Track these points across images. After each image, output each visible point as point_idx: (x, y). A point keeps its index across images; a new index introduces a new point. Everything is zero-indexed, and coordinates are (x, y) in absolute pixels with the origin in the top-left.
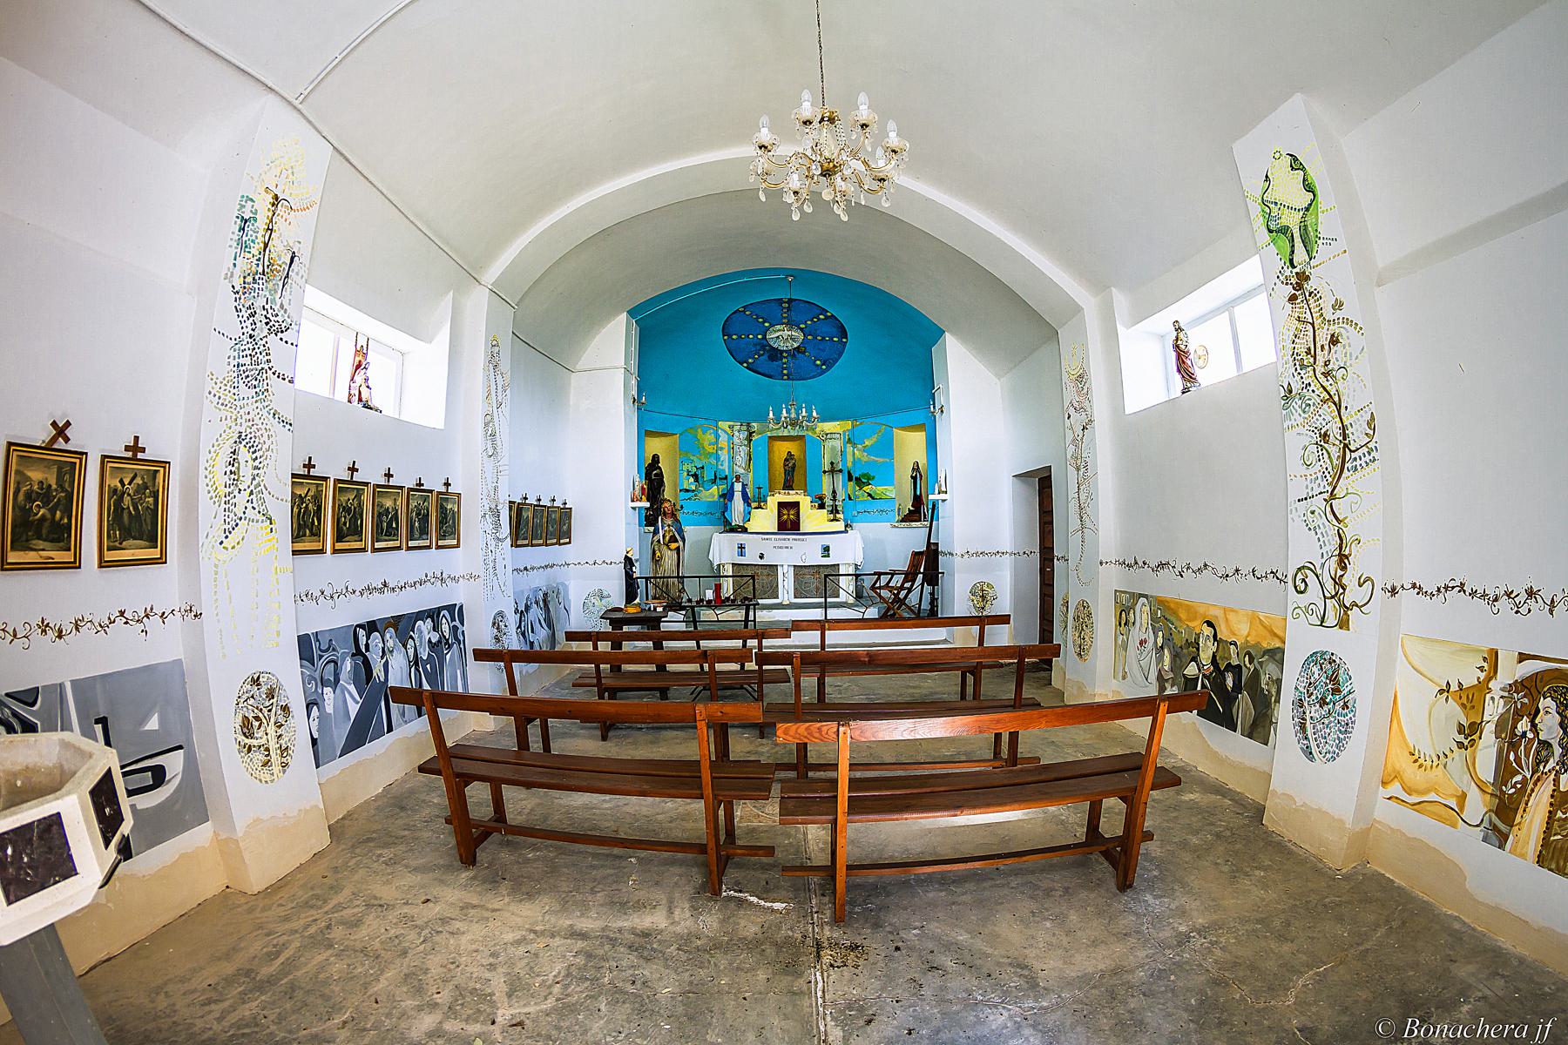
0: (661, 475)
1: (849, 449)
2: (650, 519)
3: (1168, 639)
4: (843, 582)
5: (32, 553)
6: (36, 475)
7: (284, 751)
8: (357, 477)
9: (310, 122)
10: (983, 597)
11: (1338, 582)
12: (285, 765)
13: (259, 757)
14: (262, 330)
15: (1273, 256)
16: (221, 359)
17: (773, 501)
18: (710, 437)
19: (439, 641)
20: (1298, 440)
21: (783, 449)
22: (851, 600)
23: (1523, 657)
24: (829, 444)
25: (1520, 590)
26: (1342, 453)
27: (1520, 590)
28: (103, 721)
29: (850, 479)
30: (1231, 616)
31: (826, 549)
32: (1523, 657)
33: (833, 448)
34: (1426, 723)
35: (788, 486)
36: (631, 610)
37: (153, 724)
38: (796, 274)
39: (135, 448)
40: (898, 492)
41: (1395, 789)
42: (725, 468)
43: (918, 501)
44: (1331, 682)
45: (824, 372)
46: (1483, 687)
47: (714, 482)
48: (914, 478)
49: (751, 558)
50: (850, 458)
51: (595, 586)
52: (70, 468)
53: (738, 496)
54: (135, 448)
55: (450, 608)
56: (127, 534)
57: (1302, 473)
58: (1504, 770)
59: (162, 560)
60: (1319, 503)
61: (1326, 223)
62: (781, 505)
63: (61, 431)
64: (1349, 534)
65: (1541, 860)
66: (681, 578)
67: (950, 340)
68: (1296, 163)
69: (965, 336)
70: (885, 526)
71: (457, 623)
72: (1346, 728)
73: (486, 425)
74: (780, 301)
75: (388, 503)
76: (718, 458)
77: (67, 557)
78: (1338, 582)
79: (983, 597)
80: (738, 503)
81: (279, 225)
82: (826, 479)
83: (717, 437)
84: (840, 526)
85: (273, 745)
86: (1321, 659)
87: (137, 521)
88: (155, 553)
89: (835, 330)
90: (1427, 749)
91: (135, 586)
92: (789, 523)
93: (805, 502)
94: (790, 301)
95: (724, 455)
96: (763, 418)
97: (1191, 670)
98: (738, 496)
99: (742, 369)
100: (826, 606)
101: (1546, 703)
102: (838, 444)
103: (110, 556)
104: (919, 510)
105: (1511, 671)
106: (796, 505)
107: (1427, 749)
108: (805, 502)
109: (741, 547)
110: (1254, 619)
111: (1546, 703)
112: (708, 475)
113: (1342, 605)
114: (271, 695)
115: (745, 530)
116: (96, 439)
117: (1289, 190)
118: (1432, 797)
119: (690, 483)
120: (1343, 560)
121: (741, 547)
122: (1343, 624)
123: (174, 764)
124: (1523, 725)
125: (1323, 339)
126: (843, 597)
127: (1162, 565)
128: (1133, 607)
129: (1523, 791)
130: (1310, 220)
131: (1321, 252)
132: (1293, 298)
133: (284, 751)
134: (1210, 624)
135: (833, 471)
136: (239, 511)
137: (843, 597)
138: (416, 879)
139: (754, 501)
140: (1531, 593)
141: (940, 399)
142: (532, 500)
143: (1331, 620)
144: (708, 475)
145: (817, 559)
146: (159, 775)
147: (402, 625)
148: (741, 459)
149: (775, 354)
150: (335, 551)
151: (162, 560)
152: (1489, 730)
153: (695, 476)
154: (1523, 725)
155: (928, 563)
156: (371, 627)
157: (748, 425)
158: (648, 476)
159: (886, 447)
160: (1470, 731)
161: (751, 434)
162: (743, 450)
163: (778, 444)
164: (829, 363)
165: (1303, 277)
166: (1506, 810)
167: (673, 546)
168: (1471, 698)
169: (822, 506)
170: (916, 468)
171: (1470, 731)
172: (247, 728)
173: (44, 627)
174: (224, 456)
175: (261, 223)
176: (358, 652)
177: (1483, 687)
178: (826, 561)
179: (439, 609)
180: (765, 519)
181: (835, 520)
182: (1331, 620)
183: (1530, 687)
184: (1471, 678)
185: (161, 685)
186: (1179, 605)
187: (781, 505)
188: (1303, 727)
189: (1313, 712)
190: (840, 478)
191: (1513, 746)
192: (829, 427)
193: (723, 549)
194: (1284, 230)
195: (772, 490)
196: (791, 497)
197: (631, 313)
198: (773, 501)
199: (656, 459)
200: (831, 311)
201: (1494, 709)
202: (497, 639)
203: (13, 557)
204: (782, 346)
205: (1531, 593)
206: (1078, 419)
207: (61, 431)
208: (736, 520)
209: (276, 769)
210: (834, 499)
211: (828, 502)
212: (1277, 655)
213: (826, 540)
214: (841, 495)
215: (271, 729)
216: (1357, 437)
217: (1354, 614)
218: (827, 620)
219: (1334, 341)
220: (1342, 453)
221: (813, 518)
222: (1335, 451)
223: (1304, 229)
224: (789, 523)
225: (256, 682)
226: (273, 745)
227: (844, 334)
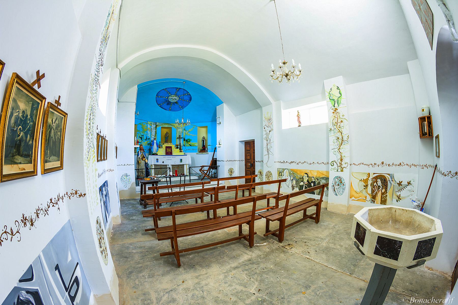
1: (184, 132)
3: (294, 178)
5: (15, 166)
11: (341, 164)
15: (331, 104)
20: (332, 138)
21: (165, 131)
23: (374, 174)
24: (179, 130)
25: (373, 163)
26: (341, 141)
27: (373, 163)
29: (184, 140)
30: (312, 172)
31: (181, 160)
32: (374, 174)
33: (180, 131)
34: (358, 186)
35: (166, 142)
40: (198, 144)
41: (353, 198)
42: (149, 136)
44: (340, 182)
46: (368, 179)
48: (203, 141)
49: (160, 163)
50: (184, 134)
51: (124, 173)
57: (333, 144)
58: (373, 191)
60: (337, 150)
61: (343, 100)
62: (166, 147)
64: (343, 155)
65: (381, 203)
67: (224, 104)
68: (338, 88)
72: (344, 189)
78: (341, 164)
80: (155, 146)
82: (178, 140)
84: (182, 154)
86: (337, 177)
90: (358, 191)
92: (169, 152)
93: (173, 147)
95: (149, 132)
97: (302, 184)
98: (155, 144)
101: (379, 180)
102: (181, 130)
105: (372, 176)
107: (358, 191)
109: (157, 160)
110: (318, 172)
111: (379, 180)
113: (341, 167)
115: (157, 155)
117: (336, 93)
118: (360, 198)
120: (341, 160)
121: (157, 160)
122: (342, 171)
124: (375, 184)
125: (339, 121)
127: (292, 162)
128: (283, 172)
129: (376, 194)
130: (339, 99)
131: (341, 105)
132: (333, 113)
134: (306, 174)
135: (180, 138)
139: (159, 146)
140: (375, 164)
143: (339, 170)
144: (145, 138)
145: (178, 163)
149: (169, 103)
152: (369, 186)
153: (141, 138)
154: (375, 184)
155: (214, 164)
159: (196, 132)
160: (366, 186)
161: (156, 126)
162: (154, 130)
165: (336, 109)
166: (374, 198)
167: (144, 159)
168: (366, 181)
169: (177, 148)
170: (204, 138)
171: (366, 186)
177: (368, 179)
178: (181, 164)
180: (162, 151)
181: (181, 152)
182: (339, 170)
183: (376, 178)
184: (365, 178)
186: (297, 170)
187: (166, 147)
188: (334, 190)
189: (336, 187)
190: (182, 140)
191: (374, 187)
194: (333, 100)
196: (169, 145)
198: (164, 146)
201: (370, 182)
203: (7, 170)
205: (375, 164)
206: (268, 129)
208: (154, 151)
212: (327, 179)
213: (181, 157)
216: (345, 139)
217: (344, 169)
219: (342, 122)
220: (341, 141)
221: (175, 151)
222: (340, 141)
223: (338, 101)
227: (190, 99)
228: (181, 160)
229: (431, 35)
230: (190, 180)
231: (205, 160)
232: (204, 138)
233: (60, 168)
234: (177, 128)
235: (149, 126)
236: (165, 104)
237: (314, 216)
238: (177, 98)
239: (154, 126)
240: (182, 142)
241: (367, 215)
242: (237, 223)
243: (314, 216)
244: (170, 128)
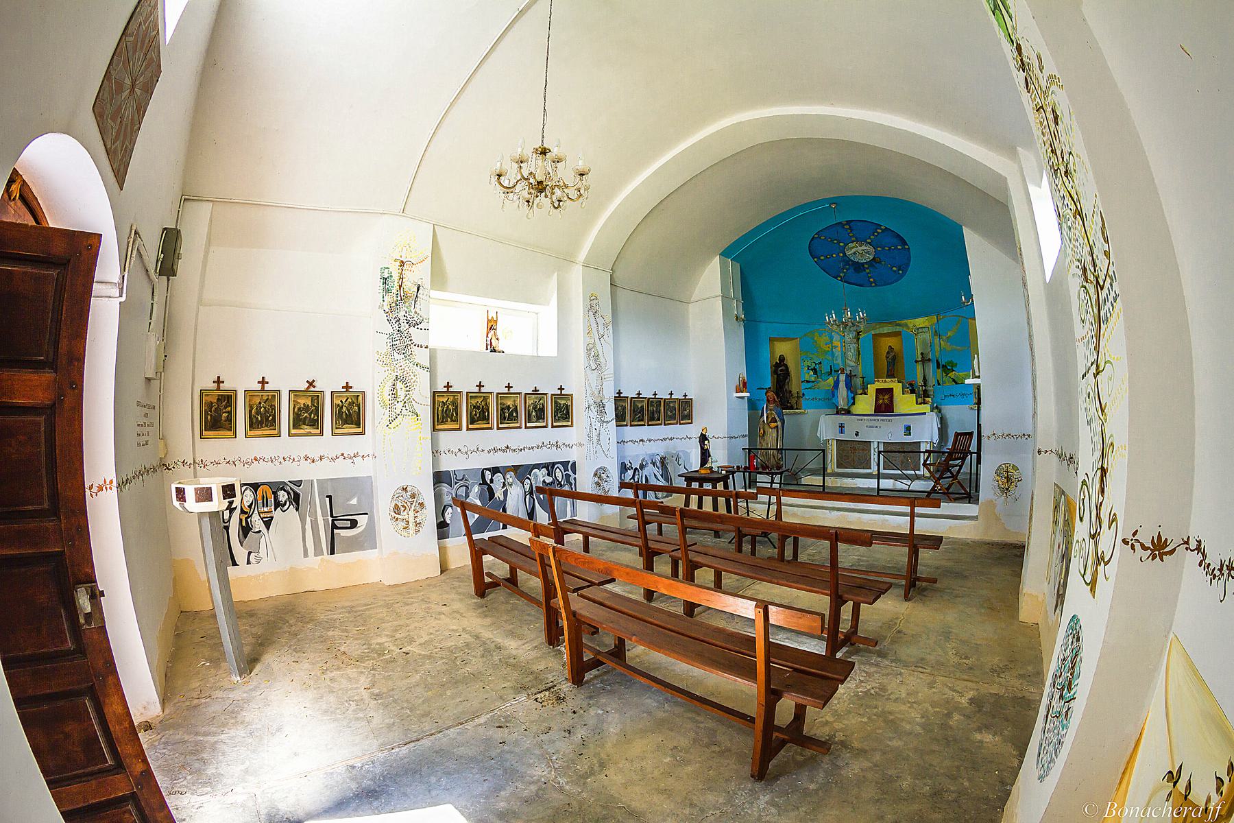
1: (937, 340)
6: (302, 401)
7: (418, 524)
8: (483, 390)
10: (1008, 478)
12: (417, 531)
13: (402, 524)
14: (404, 326)
16: (383, 345)
17: (872, 389)
18: (825, 338)
19: (553, 482)
24: (921, 337)
28: (330, 497)
29: (938, 367)
31: (908, 429)
35: (891, 375)
36: (703, 472)
37: (354, 501)
38: (837, 202)
39: (347, 387)
42: (839, 362)
45: (902, 276)
50: (937, 348)
52: (317, 398)
53: (842, 385)
54: (347, 387)
55: (565, 464)
56: (345, 422)
59: (363, 433)
62: (878, 391)
63: (311, 384)
69: (975, 228)
71: (570, 472)
73: (589, 350)
74: (879, 226)
75: (510, 403)
76: (833, 355)
77: (318, 431)
79: (1008, 478)
81: (407, 274)
83: (832, 338)
85: (411, 520)
87: (351, 415)
88: (360, 430)
89: (895, 241)
91: (349, 443)
92: (885, 405)
93: (897, 387)
94: (848, 222)
95: (838, 352)
100: (879, 477)
103: (336, 431)
106: (890, 391)
108: (897, 387)
109: (842, 426)
114: (413, 496)
119: (810, 375)
121: (842, 426)
123: (362, 521)
133: (418, 524)
135: (925, 360)
136: (398, 411)
138: (457, 597)
139: (855, 388)
142: (678, 395)
145: (899, 437)
146: (354, 524)
147: (522, 472)
148: (851, 355)
149: (858, 267)
150: (468, 429)
151: (363, 433)
153: (815, 370)
156: (495, 470)
162: (853, 347)
163: (883, 339)
164: (904, 267)
167: (773, 425)
172: (397, 510)
173: (306, 458)
174: (390, 384)
175: (396, 277)
176: (484, 482)
179: (554, 464)
180: (865, 404)
181: (924, 403)
185: (361, 486)
187: (878, 391)
190: (931, 367)
193: (827, 428)
195: (878, 376)
197: (725, 254)
198: (872, 389)
199: (782, 359)
200: (885, 224)
202: (598, 484)
207: (311, 384)
209: (412, 532)
210: (925, 384)
214: (932, 381)
215: (411, 513)
218: (879, 489)
221: (905, 402)
224: (885, 405)
225: (405, 489)
226: (411, 520)
227: (904, 242)
228: (908, 429)
229: (115, 61)
230: (879, 489)
237: (487, 580)
239: (850, 337)
240: (933, 374)
242: (514, 560)
243: (487, 580)
244: (898, 334)
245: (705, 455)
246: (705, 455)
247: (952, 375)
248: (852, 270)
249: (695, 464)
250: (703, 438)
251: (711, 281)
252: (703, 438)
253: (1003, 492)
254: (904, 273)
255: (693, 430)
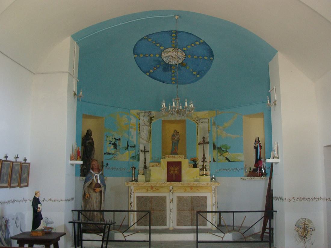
0: (92, 144)
1: (214, 128)
2: (85, 171)
4: (209, 216)
9: (219, 236)
21: (171, 128)
22: (214, 228)
24: (201, 126)
29: (214, 147)
35: (174, 152)
36: (34, 234)
42: (133, 141)
43: (258, 161)
45: (198, 79)
47: (127, 148)
48: (256, 148)
62: (170, 164)
66: (102, 211)
67: (278, 52)
70: (238, 179)
76: (129, 133)
82: (200, 148)
92: (174, 174)
94: (177, 32)
95: (133, 132)
96: (158, 108)
99: (146, 77)
102: (206, 126)
104: (259, 169)
106: (179, 164)
112: (123, 144)
116: (9, 204)
119: (111, 149)
126: (209, 226)
135: (204, 143)
137: (209, 226)
139: (157, 161)
141: (274, 96)
142: (20, 160)
144: (123, 144)
149: (167, 67)
153: (115, 145)
157: (150, 113)
158: (83, 144)
161: (151, 118)
167: (98, 190)
169: (195, 166)
170: (257, 141)
180: (159, 173)
187: (170, 164)
190: (208, 148)
192: (201, 114)
197: (75, 37)
198: (164, 163)
204: (172, 62)
211: (200, 163)
214: (208, 158)
218: (198, 242)
221: (189, 173)
231: (248, 193)
232: (257, 141)
233: (27, 186)
234: (198, 121)
235: (133, 121)
236: (162, 71)
238: (181, 54)
239: (146, 119)
241: (224, 224)
244: (184, 121)
245: (37, 217)
246: (37, 217)
247: (226, 155)
248: (161, 69)
249: (28, 227)
250: (36, 202)
251: (63, 55)
252: (36, 202)
253: (302, 239)
254: (201, 77)
255: (25, 194)
